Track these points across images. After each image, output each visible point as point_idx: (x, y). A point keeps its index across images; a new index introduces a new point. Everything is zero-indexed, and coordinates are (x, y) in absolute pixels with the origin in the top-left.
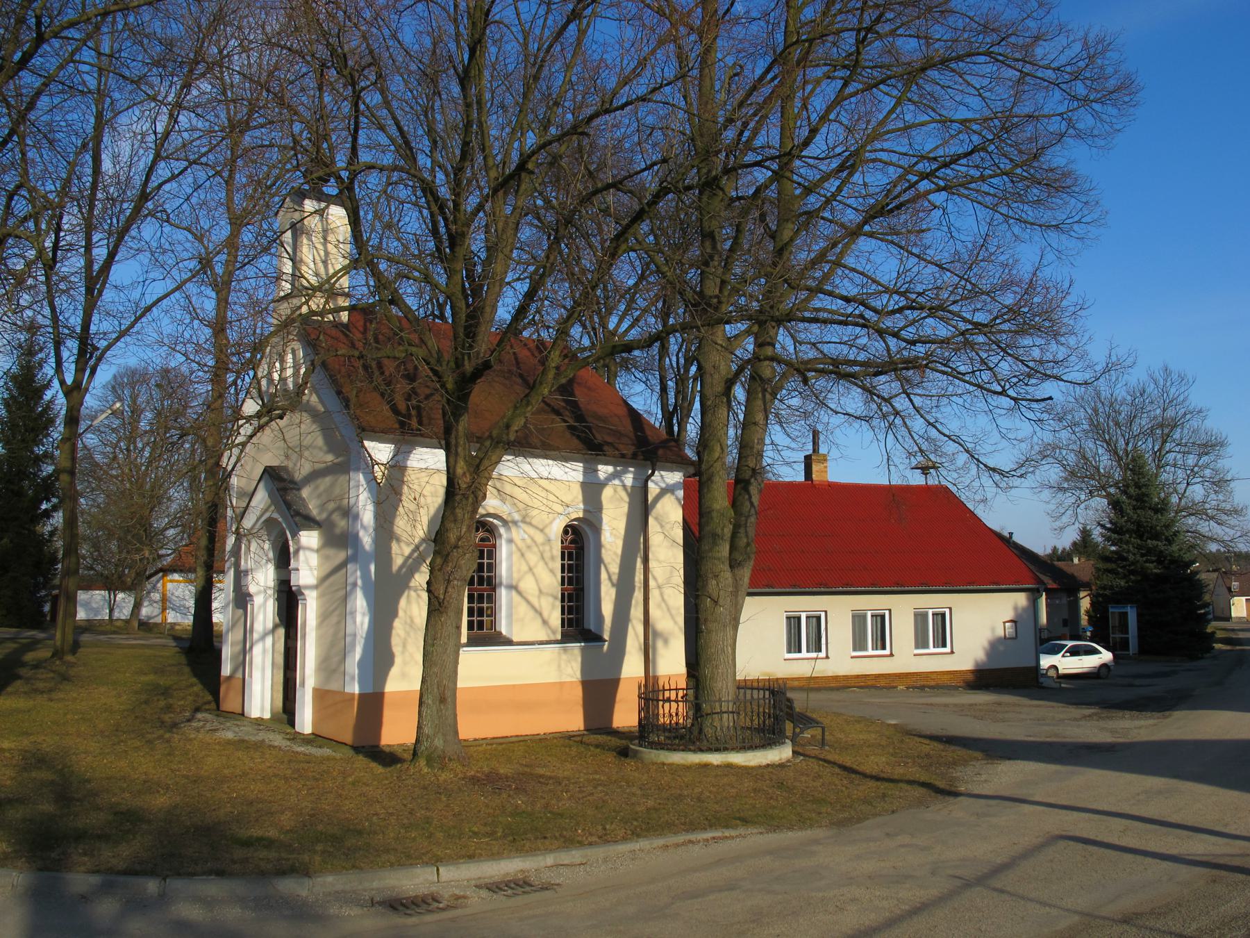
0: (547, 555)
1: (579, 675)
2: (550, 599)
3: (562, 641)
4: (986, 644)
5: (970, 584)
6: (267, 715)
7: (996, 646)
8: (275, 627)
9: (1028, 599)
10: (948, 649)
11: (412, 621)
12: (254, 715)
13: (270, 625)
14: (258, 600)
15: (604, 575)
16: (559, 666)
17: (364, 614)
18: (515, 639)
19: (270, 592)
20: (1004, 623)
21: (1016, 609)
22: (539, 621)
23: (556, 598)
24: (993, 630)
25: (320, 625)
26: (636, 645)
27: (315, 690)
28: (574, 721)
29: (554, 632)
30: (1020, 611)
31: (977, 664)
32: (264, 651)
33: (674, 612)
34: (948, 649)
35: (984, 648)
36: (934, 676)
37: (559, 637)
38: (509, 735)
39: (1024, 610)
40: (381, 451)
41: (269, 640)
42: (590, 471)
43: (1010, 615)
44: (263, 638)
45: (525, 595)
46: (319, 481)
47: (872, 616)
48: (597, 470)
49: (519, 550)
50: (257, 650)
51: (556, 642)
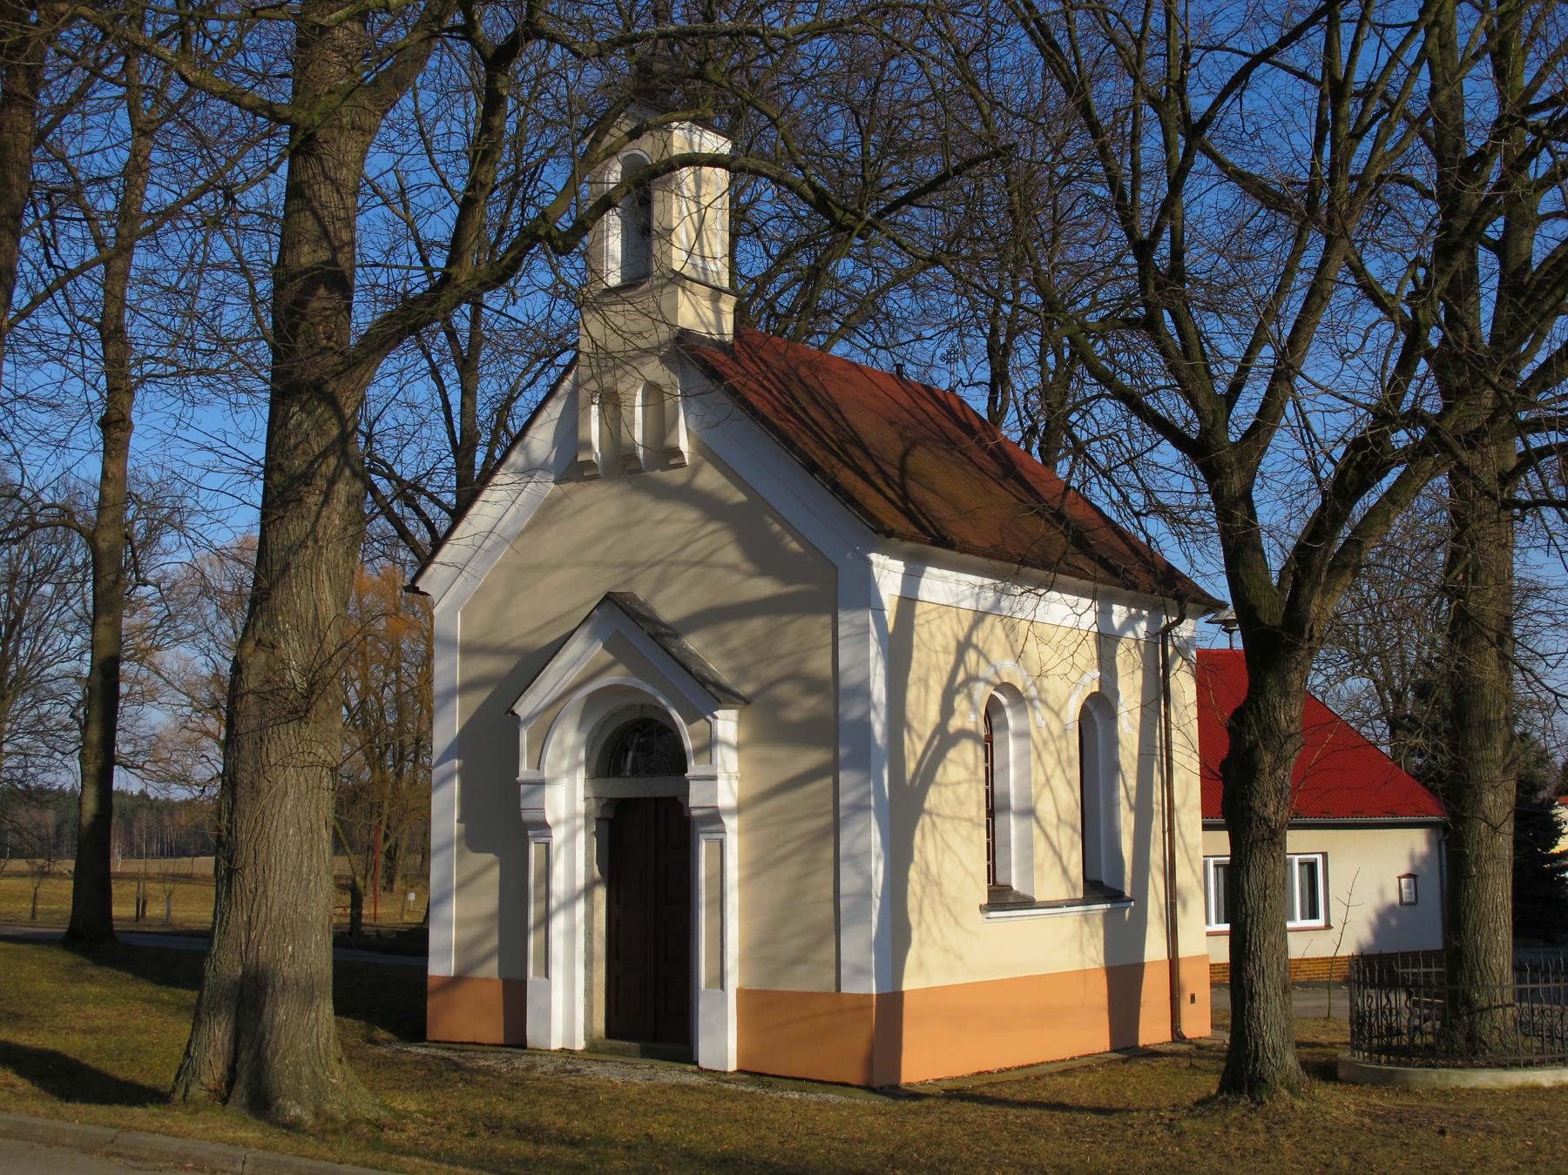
0: (1064, 756)
1: (1102, 962)
2: (1069, 831)
3: (1085, 902)
4: (1372, 916)
5: (1355, 814)
6: (580, 1045)
7: (1386, 919)
8: (588, 890)
9: (1429, 842)
10: (1320, 922)
11: (928, 867)
12: (556, 1043)
13: (580, 882)
14: (558, 835)
15: (1122, 792)
16: (1081, 945)
17: (878, 858)
18: (1039, 897)
19: (580, 822)
20: (1399, 878)
21: (1412, 857)
22: (1058, 870)
23: (1074, 829)
24: (1382, 892)
25: (744, 882)
26: (1157, 911)
27: (743, 994)
28: (1095, 1038)
29: (1074, 888)
30: (1418, 861)
31: (1360, 946)
32: (571, 933)
33: (1191, 853)
34: (1320, 922)
35: (1370, 923)
36: (1304, 966)
37: (1080, 895)
38: (1034, 1061)
39: (1424, 859)
40: (888, 573)
41: (580, 908)
42: (1104, 615)
43: (1405, 868)
44: (569, 903)
45: (1043, 824)
46: (730, 627)
47: (1301, 864)
48: (1111, 612)
49: (1036, 747)
50: (558, 924)
51: (1071, 903)
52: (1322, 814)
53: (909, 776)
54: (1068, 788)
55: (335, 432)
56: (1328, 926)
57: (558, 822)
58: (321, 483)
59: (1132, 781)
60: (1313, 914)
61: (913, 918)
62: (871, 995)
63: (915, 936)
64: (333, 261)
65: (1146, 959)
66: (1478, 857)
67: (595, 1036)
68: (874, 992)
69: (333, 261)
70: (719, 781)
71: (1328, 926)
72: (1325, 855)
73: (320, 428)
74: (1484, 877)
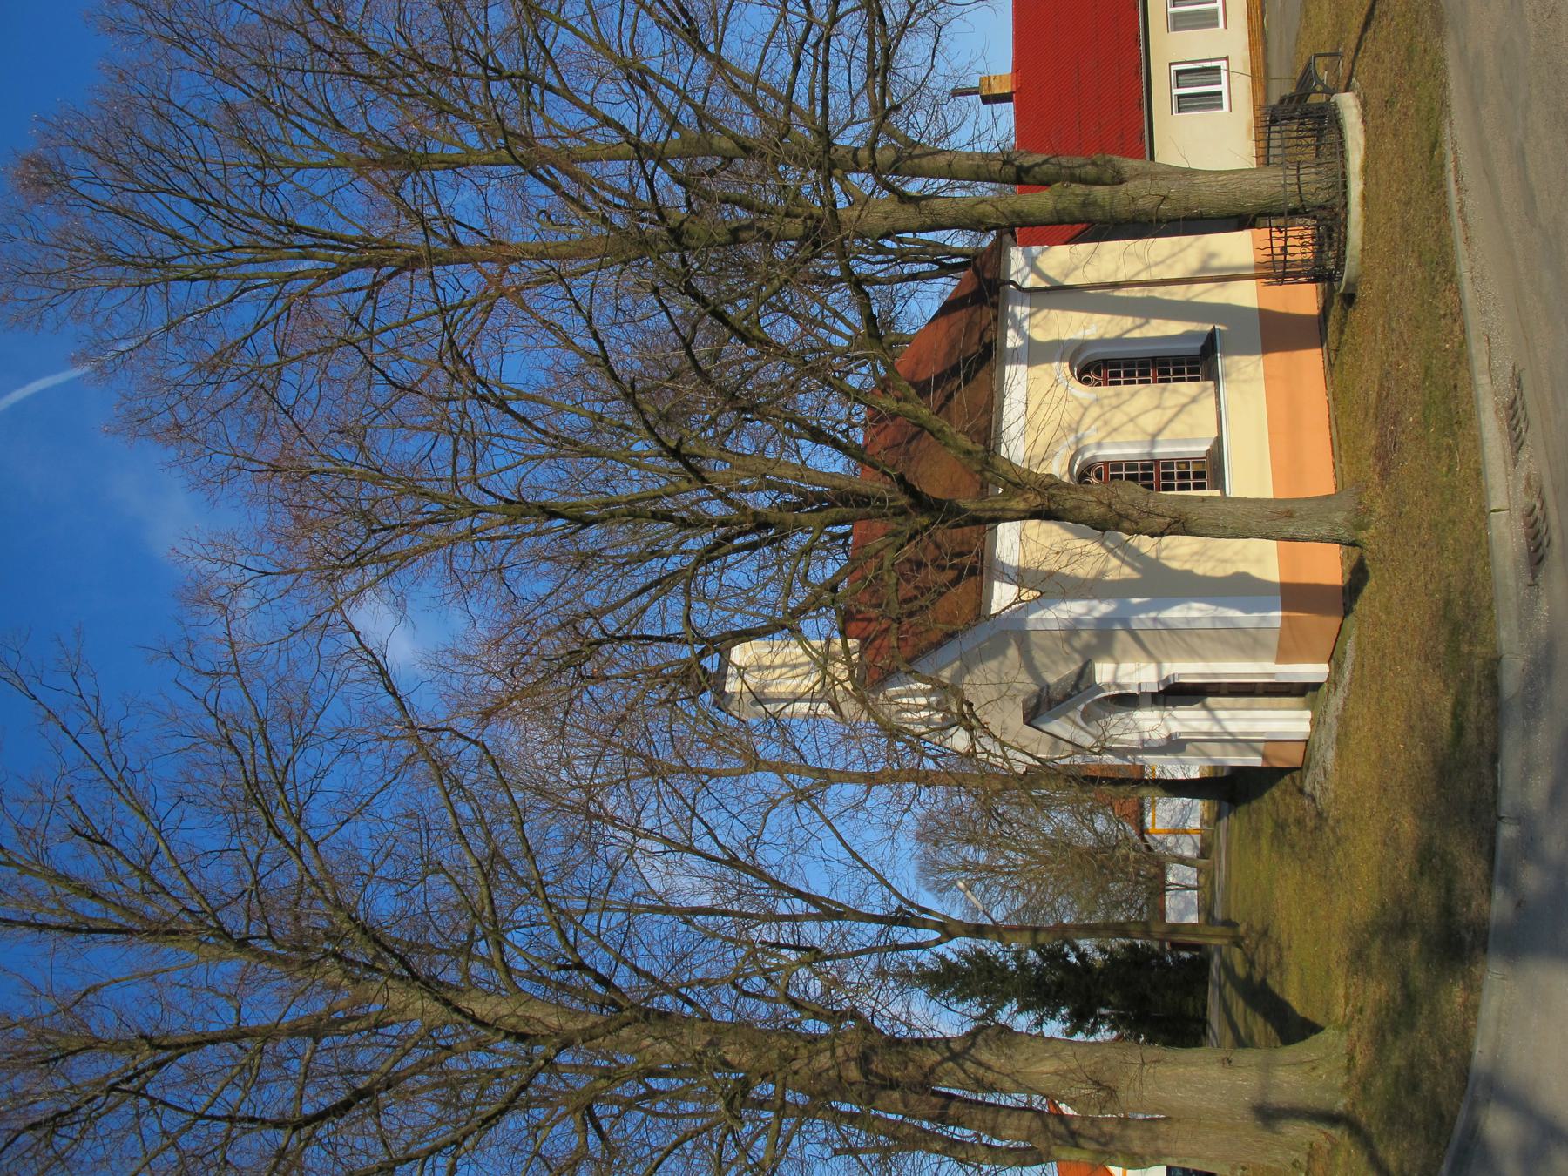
0: (1114, 401)
1: (1257, 357)
2: (1166, 394)
6: (1308, 714)
8: (1205, 707)
11: (1196, 553)
13: (1203, 713)
14: (1175, 727)
15: (1136, 334)
16: (1245, 381)
18: (1215, 434)
19: (1166, 714)
22: (1193, 407)
23: (1164, 389)
27: (1279, 660)
28: (1311, 360)
29: (1205, 389)
32: (1232, 719)
34: (1223, 64)
37: (1211, 383)
40: (1003, 595)
42: (1015, 356)
44: (1218, 721)
45: (1161, 425)
49: (1109, 434)
50: (1233, 727)
51: (1217, 386)
52: (1140, 105)
53: (1135, 575)
54: (1136, 397)
55: (951, 1064)
56: (1226, 59)
57: (1168, 728)
58: (981, 1071)
59: (1128, 322)
60: (1218, 69)
61: (1229, 570)
62: (1283, 617)
63: (1242, 568)
64: (855, 1059)
65: (1255, 305)
66: (1186, 209)
67: (1302, 705)
68: (1279, 614)
69: (855, 1059)
70: (1142, 681)
71: (1226, 59)
72: (1171, 64)
73: (947, 1073)
74: (1200, 204)
